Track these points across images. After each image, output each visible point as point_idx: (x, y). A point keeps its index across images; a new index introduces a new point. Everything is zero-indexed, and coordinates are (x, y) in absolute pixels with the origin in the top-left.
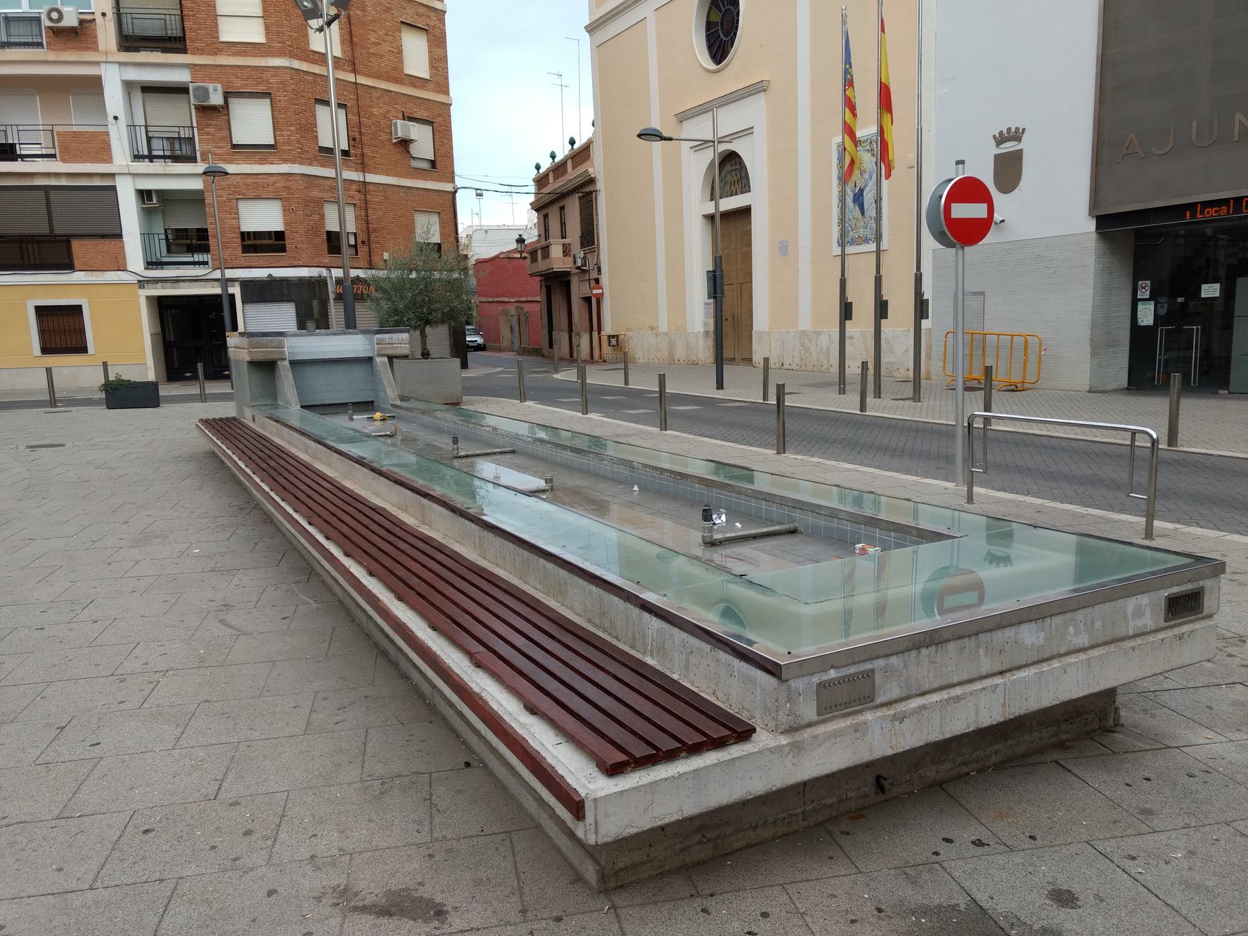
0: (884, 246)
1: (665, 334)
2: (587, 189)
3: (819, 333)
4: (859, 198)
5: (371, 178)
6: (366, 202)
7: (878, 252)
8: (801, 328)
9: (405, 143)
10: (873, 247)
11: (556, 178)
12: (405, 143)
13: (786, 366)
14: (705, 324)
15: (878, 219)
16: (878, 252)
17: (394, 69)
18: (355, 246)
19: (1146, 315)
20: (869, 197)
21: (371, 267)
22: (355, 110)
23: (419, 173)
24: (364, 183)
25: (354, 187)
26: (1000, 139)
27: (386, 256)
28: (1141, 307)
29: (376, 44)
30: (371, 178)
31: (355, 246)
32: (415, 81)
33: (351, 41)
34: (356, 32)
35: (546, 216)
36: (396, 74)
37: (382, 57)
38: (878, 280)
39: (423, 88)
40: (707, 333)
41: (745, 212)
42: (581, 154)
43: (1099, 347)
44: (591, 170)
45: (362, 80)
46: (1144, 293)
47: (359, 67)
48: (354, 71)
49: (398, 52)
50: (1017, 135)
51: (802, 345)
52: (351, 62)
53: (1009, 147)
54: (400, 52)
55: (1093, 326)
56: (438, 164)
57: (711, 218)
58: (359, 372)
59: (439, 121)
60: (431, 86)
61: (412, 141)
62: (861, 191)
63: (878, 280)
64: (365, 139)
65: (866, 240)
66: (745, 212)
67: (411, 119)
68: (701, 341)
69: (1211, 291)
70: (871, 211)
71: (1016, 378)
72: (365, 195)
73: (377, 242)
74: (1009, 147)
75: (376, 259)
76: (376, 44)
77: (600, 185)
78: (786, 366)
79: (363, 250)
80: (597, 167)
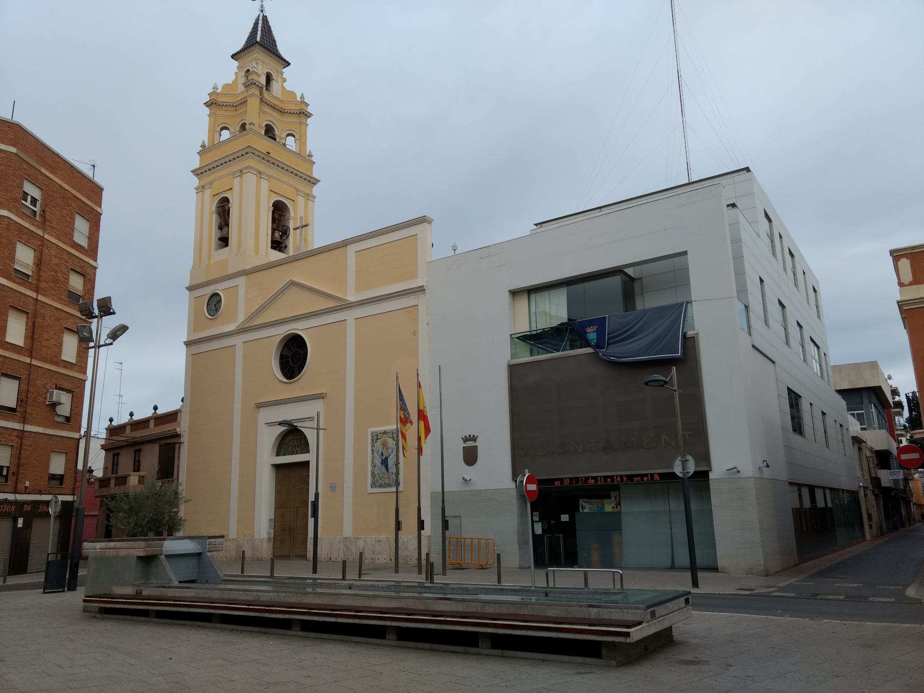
0: (401, 488)
1: (235, 540)
2: (172, 441)
3: (357, 539)
4: (385, 462)
5: (28, 428)
6: (21, 444)
7: (397, 492)
8: (345, 536)
9: (54, 405)
10: (394, 489)
11: (132, 430)
12: (54, 405)
13: (333, 559)
14: (269, 533)
15: (397, 474)
16: (397, 492)
17: (56, 356)
18: (6, 477)
19: (539, 530)
20: (391, 462)
21: (15, 492)
22: (26, 381)
23: (59, 426)
24: (23, 431)
25: (15, 434)
26: (466, 440)
27: (27, 484)
28: (535, 525)
29: (47, 340)
30: (28, 428)
31: (6, 477)
32: (67, 365)
33: (32, 337)
34: (36, 332)
35: (116, 455)
36: (56, 359)
37: (49, 348)
38: (443, 509)
39: (71, 369)
40: (269, 539)
41: (307, 464)
42: (172, 417)
43: (522, 544)
44: (178, 429)
45: (34, 362)
46: (536, 518)
47: (34, 354)
48: (31, 357)
49: (60, 346)
50: (474, 439)
51: (345, 546)
52: (30, 349)
53: (470, 444)
54: (61, 345)
55: (519, 535)
56: (72, 419)
57: (278, 467)
58: (192, 562)
59: (76, 390)
60: (76, 368)
61: (60, 404)
62: (387, 458)
63: (443, 509)
64: (30, 401)
65: (390, 485)
66: (307, 464)
67: (60, 389)
68: (265, 544)
69: (565, 518)
70: (393, 469)
71: (483, 562)
72: (22, 439)
73: (23, 474)
74: (470, 444)
75: (20, 487)
76: (47, 340)
77: (185, 439)
78: (333, 559)
79: (12, 479)
80: (183, 427)
